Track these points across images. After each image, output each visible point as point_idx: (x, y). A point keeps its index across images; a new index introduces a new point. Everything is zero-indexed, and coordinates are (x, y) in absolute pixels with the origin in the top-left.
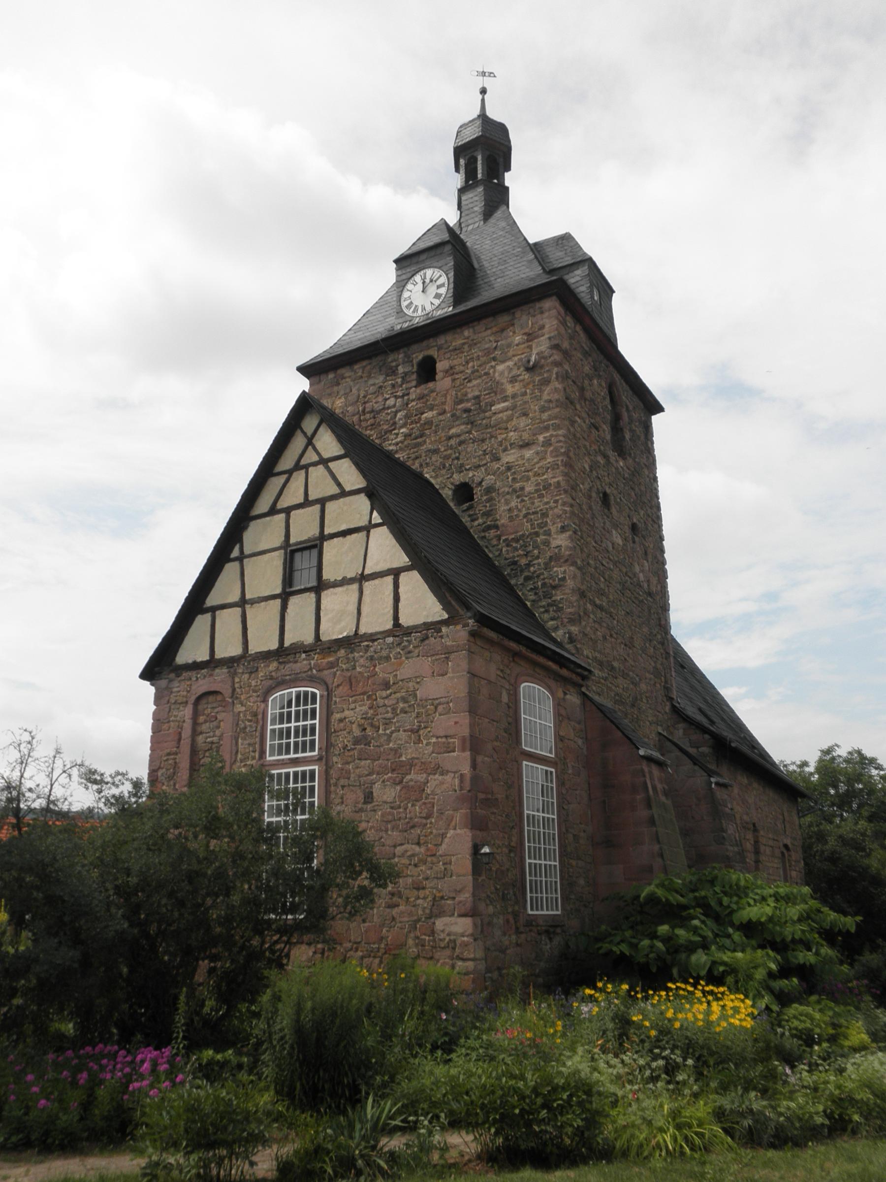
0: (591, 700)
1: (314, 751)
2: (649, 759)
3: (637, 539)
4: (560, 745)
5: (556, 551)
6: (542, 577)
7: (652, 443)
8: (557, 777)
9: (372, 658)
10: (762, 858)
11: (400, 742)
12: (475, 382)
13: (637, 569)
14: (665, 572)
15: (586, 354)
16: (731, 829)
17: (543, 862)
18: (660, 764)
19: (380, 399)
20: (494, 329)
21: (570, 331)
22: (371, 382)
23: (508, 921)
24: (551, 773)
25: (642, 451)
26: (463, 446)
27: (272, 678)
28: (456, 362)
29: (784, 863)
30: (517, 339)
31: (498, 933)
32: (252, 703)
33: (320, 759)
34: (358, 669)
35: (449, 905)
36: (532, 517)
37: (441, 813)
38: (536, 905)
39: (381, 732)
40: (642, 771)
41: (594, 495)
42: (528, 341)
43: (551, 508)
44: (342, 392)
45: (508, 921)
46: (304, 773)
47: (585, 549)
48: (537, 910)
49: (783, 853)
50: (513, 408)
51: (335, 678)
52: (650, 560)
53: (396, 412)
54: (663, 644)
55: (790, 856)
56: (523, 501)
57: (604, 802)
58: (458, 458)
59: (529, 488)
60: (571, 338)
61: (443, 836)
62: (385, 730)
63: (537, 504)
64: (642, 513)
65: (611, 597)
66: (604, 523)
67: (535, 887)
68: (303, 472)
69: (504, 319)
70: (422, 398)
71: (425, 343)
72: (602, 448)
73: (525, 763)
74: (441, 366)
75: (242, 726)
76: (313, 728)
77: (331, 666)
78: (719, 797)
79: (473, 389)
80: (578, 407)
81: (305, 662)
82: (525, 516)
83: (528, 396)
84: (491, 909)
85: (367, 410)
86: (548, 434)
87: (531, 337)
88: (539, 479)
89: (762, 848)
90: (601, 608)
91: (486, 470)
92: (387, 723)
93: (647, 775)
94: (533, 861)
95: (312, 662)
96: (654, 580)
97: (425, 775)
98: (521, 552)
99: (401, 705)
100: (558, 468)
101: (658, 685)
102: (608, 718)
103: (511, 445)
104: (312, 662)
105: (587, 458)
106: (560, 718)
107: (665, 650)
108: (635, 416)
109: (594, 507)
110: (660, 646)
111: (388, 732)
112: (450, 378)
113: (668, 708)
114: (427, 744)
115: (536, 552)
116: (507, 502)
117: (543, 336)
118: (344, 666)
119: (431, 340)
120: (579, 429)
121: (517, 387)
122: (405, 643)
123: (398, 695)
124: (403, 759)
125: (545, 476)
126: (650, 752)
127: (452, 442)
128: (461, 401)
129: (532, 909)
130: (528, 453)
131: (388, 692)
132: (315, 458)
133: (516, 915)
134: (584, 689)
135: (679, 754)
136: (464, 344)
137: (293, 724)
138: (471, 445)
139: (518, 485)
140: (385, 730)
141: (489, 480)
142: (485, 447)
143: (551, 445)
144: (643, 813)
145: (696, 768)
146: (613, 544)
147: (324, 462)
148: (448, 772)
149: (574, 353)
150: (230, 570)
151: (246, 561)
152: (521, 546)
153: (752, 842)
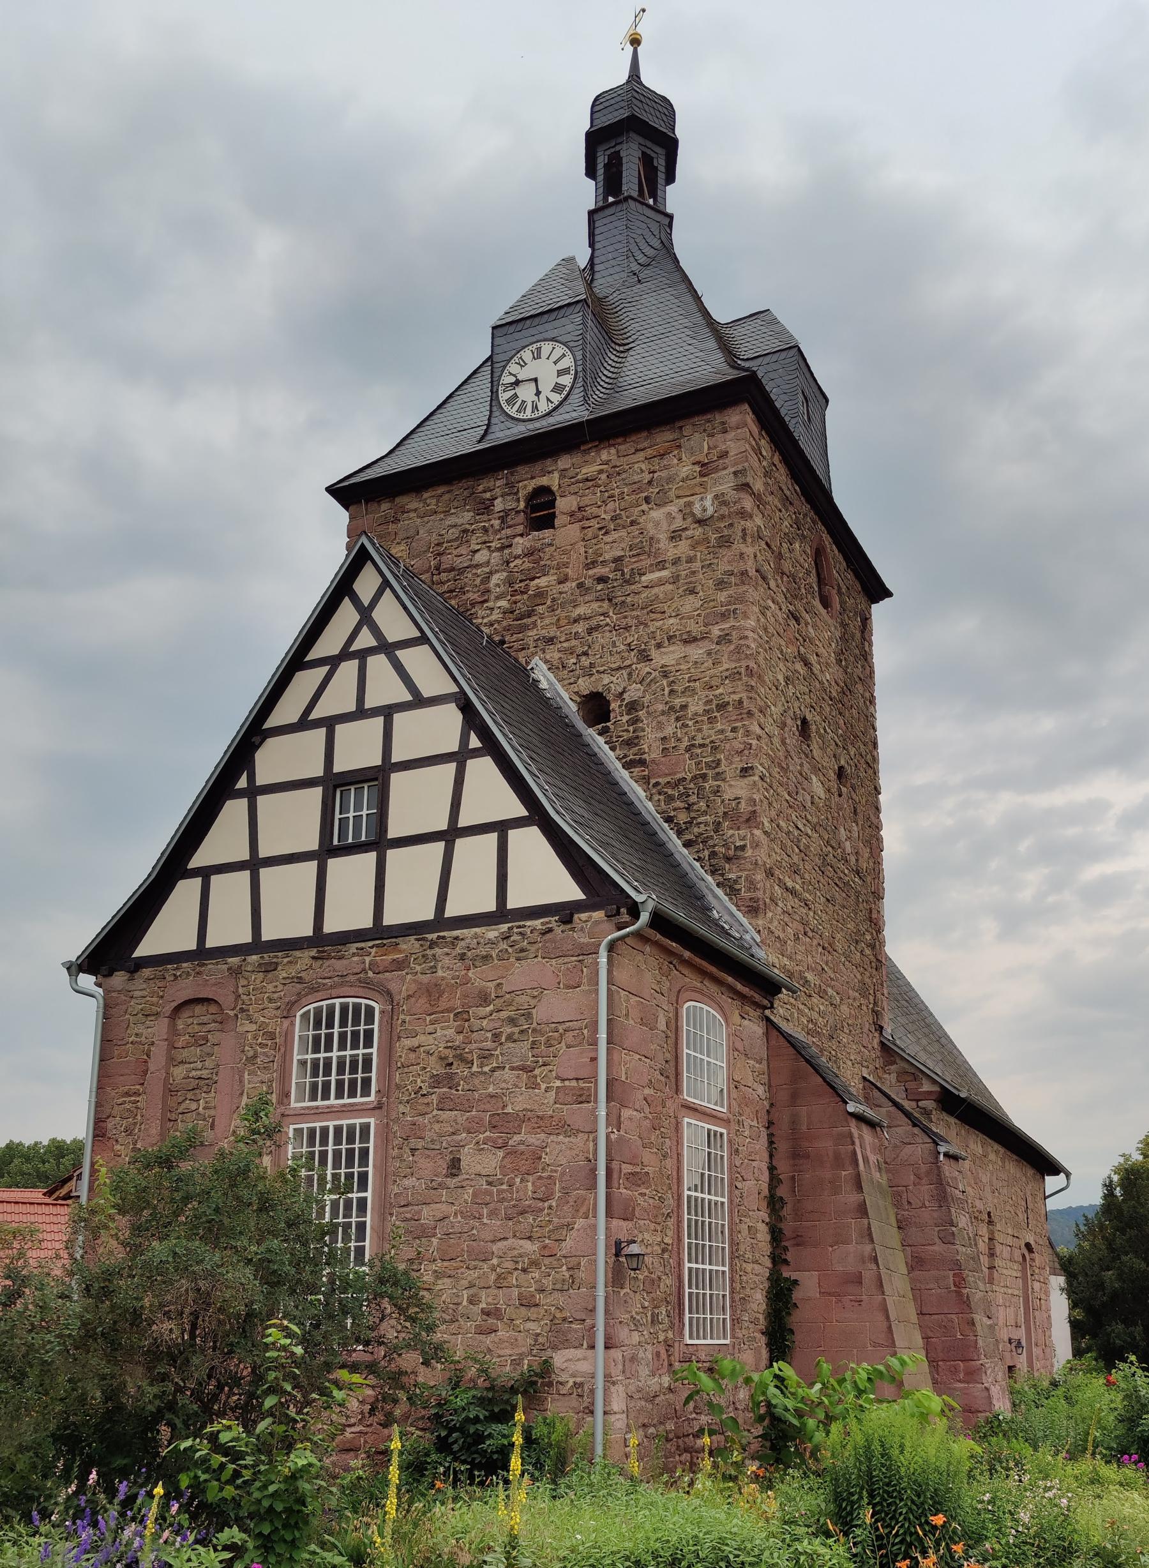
0: (778, 1029)
1: (369, 1095)
2: (859, 1118)
3: (844, 789)
4: (734, 1092)
5: (734, 804)
6: (711, 843)
7: (871, 645)
8: (730, 1141)
9: (462, 957)
10: (998, 1262)
11: (504, 1085)
12: (614, 535)
13: (843, 833)
14: (880, 840)
15: (786, 501)
16: (963, 1221)
17: (708, 1267)
18: (872, 1124)
19: (463, 550)
20: (649, 452)
21: (765, 463)
22: (452, 520)
23: (658, 1354)
24: (722, 1135)
25: (855, 656)
26: (595, 635)
27: (300, 980)
28: (586, 501)
29: (1024, 1271)
30: (685, 470)
31: (644, 1371)
32: (269, 1018)
33: (379, 1107)
34: (440, 973)
35: (576, 1331)
36: (699, 751)
37: (566, 1192)
38: (698, 1329)
39: (475, 1069)
40: (851, 1135)
41: (789, 722)
42: (702, 475)
43: (727, 739)
44: (401, 535)
45: (658, 1354)
46: (351, 1129)
47: (774, 804)
48: (698, 1338)
49: (1024, 1256)
50: (675, 579)
51: (402, 984)
52: (860, 823)
53: (491, 573)
54: (872, 947)
55: (1033, 1260)
56: (685, 726)
57: (793, 1177)
58: (585, 654)
59: (696, 706)
60: (767, 474)
61: (569, 1227)
62: (481, 1066)
63: (706, 732)
64: (852, 751)
65: (807, 876)
66: (801, 765)
67: (698, 1304)
68: (355, 663)
69: (664, 437)
70: (532, 554)
71: (538, 467)
72: (802, 650)
73: (686, 1120)
74: (563, 504)
75: (251, 1054)
76: (368, 1061)
77: (399, 965)
78: (947, 1174)
79: (614, 545)
80: (772, 584)
81: (356, 959)
82: (688, 750)
83: (698, 564)
84: (636, 1337)
85: (443, 567)
86: (727, 626)
87: (706, 468)
88: (711, 694)
89: (998, 1249)
90: (792, 892)
91: (630, 674)
92: (485, 1057)
93: (857, 1141)
94: (694, 1266)
95: (367, 959)
96: (866, 852)
97: (543, 1136)
98: (679, 804)
99: (508, 1030)
100: (740, 679)
101: (864, 1008)
102: (803, 1056)
103: (670, 638)
104: (367, 959)
105: (781, 665)
106: (737, 1052)
107: (875, 956)
108: (850, 602)
109: (788, 741)
110: (868, 952)
111: (486, 1069)
112: (577, 526)
113: (876, 1043)
114: (547, 1090)
115: (702, 804)
116: (660, 726)
117: (725, 468)
118: (418, 968)
119: (549, 462)
120: (773, 620)
121: (683, 548)
122: (515, 937)
123: (504, 1014)
124: (509, 1110)
125: (720, 691)
126: (862, 1107)
127: (580, 628)
128: (594, 564)
129: (691, 1337)
130: (696, 652)
131: (488, 1009)
132: (373, 643)
133: (669, 1346)
134: (767, 1012)
135: (893, 1109)
136: (601, 472)
137: (335, 1054)
138: (608, 634)
139: (678, 702)
140: (481, 1066)
141: (634, 692)
142: (629, 640)
143: (730, 641)
144: (853, 1198)
145: (916, 1130)
146: (812, 797)
147: (386, 648)
148: (578, 1131)
149: (770, 498)
150: (234, 811)
151: (261, 800)
152: (681, 795)
153: (987, 1240)
